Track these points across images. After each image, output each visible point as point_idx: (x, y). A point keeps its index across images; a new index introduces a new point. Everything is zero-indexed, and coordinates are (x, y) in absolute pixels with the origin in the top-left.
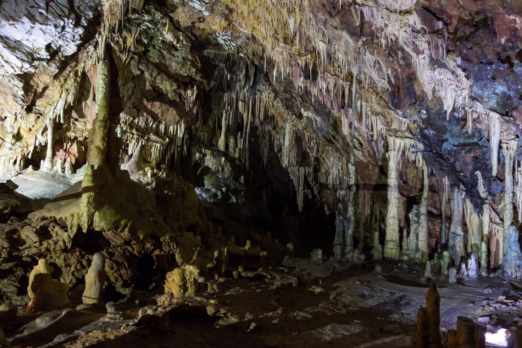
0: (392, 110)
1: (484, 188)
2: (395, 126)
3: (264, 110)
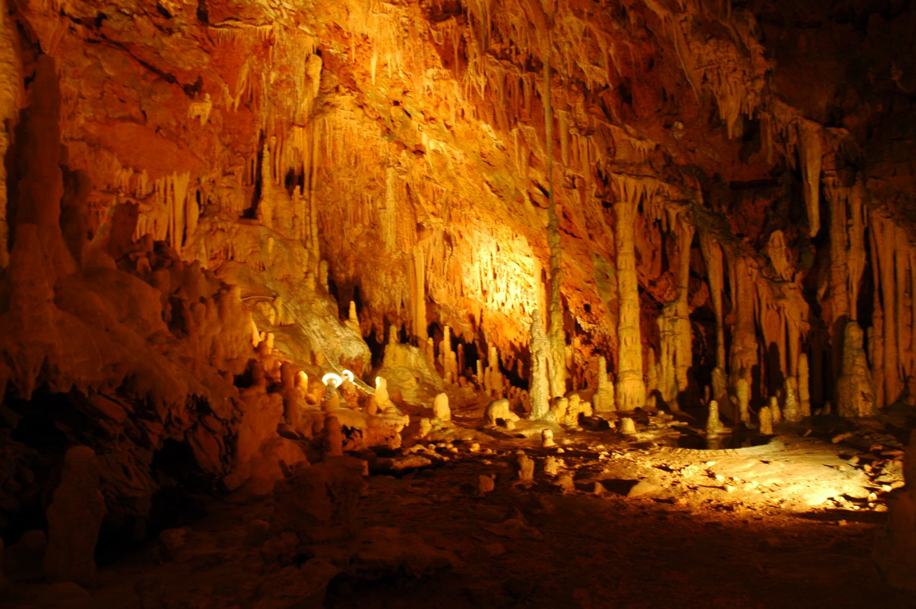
0: (617, 125)
1: (788, 260)
2: (622, 155)
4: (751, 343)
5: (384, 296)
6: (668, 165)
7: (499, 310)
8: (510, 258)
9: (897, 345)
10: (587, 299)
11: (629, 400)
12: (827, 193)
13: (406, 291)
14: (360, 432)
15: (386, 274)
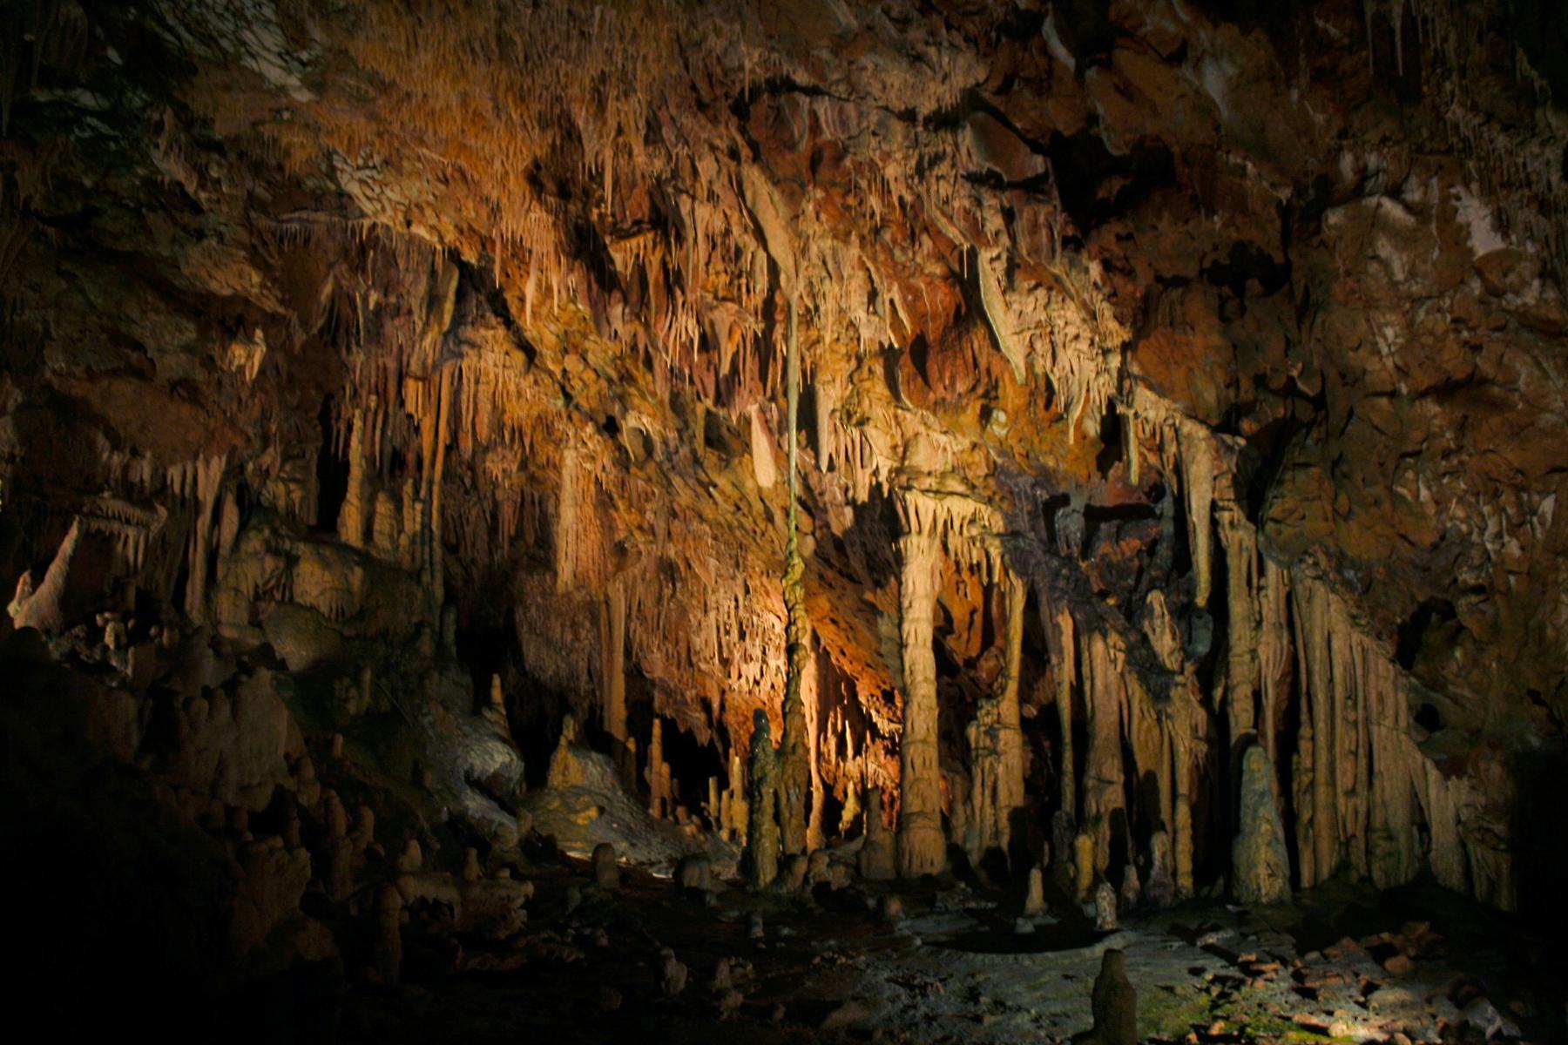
1: (1174, 639)
3: (489, 407)
4: (1112, 770)
5: (559, 662)
6: (993, 475)
7: (750, 692)
8: (766, 607)
10: (884, 683)
11: (916, 862)
12: (1222, 536)
13: (595, 654)
14: (450, 908)
15: (563, 626)
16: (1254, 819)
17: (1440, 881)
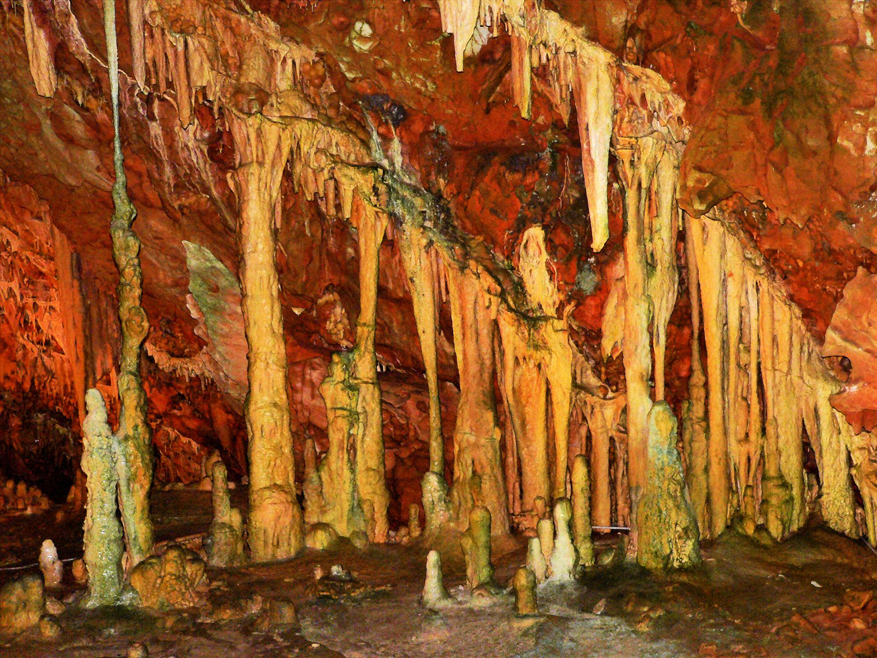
9: (725, 433)
16: (800, 64)
17: (832, 526)
